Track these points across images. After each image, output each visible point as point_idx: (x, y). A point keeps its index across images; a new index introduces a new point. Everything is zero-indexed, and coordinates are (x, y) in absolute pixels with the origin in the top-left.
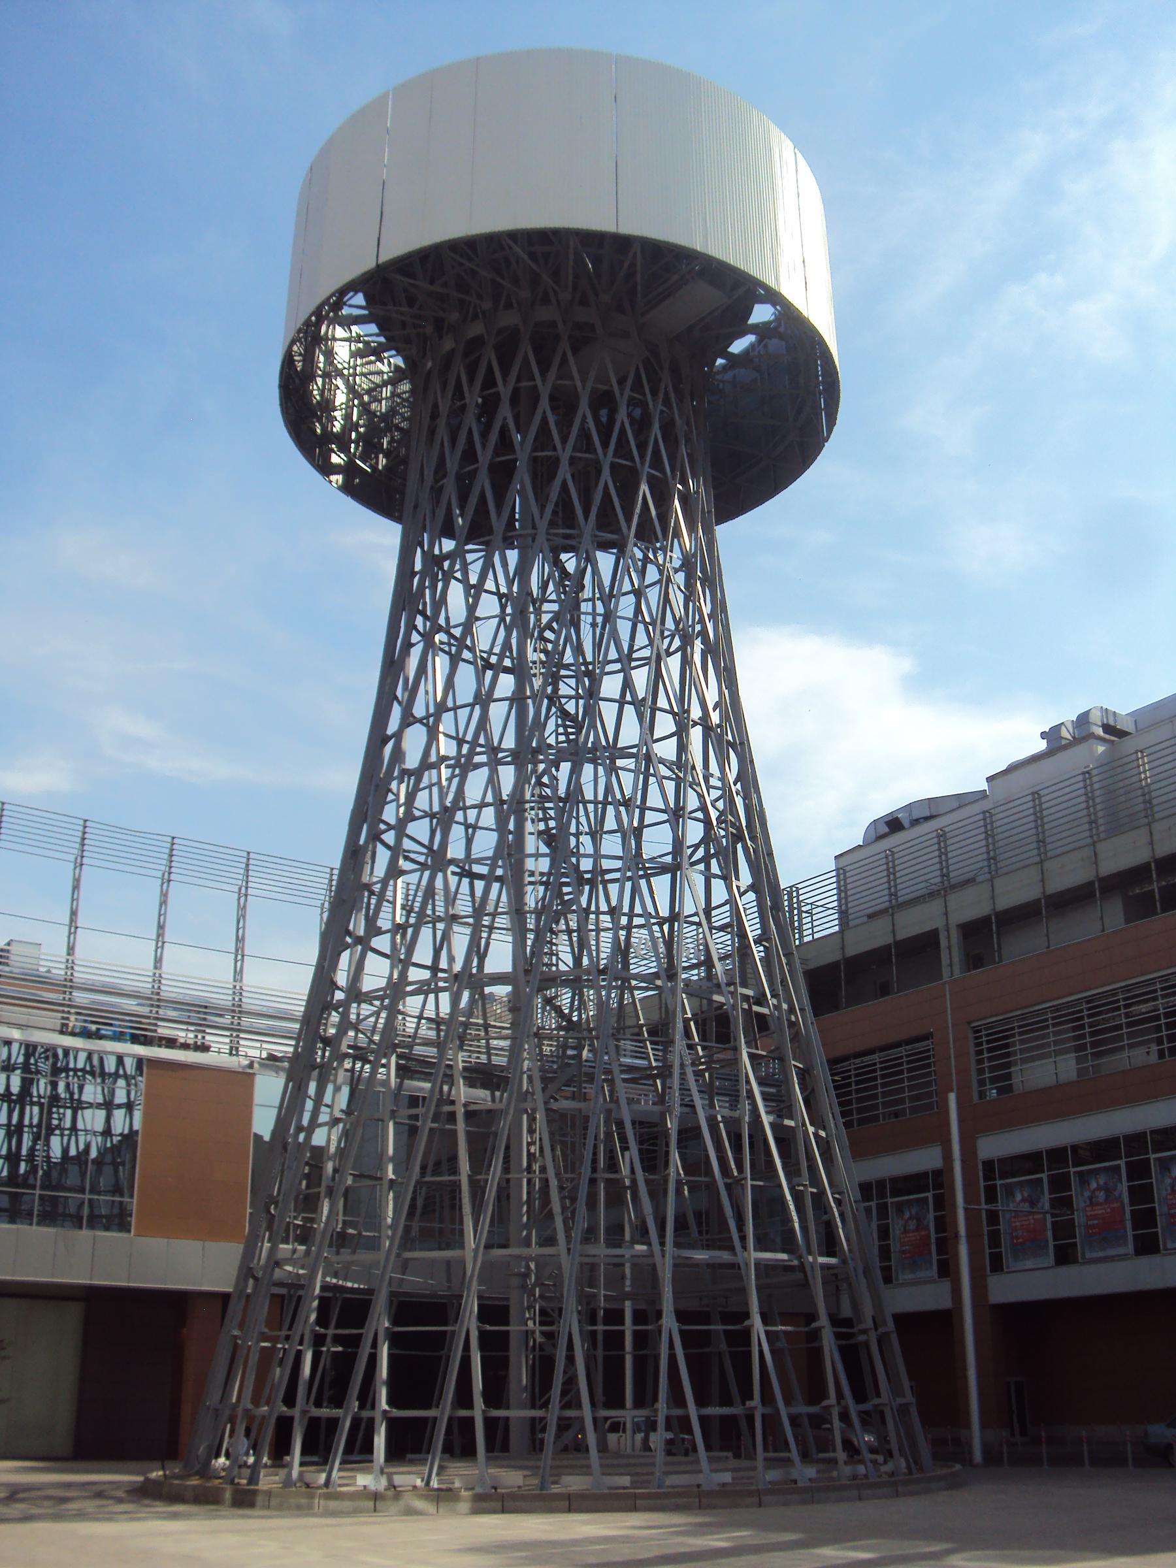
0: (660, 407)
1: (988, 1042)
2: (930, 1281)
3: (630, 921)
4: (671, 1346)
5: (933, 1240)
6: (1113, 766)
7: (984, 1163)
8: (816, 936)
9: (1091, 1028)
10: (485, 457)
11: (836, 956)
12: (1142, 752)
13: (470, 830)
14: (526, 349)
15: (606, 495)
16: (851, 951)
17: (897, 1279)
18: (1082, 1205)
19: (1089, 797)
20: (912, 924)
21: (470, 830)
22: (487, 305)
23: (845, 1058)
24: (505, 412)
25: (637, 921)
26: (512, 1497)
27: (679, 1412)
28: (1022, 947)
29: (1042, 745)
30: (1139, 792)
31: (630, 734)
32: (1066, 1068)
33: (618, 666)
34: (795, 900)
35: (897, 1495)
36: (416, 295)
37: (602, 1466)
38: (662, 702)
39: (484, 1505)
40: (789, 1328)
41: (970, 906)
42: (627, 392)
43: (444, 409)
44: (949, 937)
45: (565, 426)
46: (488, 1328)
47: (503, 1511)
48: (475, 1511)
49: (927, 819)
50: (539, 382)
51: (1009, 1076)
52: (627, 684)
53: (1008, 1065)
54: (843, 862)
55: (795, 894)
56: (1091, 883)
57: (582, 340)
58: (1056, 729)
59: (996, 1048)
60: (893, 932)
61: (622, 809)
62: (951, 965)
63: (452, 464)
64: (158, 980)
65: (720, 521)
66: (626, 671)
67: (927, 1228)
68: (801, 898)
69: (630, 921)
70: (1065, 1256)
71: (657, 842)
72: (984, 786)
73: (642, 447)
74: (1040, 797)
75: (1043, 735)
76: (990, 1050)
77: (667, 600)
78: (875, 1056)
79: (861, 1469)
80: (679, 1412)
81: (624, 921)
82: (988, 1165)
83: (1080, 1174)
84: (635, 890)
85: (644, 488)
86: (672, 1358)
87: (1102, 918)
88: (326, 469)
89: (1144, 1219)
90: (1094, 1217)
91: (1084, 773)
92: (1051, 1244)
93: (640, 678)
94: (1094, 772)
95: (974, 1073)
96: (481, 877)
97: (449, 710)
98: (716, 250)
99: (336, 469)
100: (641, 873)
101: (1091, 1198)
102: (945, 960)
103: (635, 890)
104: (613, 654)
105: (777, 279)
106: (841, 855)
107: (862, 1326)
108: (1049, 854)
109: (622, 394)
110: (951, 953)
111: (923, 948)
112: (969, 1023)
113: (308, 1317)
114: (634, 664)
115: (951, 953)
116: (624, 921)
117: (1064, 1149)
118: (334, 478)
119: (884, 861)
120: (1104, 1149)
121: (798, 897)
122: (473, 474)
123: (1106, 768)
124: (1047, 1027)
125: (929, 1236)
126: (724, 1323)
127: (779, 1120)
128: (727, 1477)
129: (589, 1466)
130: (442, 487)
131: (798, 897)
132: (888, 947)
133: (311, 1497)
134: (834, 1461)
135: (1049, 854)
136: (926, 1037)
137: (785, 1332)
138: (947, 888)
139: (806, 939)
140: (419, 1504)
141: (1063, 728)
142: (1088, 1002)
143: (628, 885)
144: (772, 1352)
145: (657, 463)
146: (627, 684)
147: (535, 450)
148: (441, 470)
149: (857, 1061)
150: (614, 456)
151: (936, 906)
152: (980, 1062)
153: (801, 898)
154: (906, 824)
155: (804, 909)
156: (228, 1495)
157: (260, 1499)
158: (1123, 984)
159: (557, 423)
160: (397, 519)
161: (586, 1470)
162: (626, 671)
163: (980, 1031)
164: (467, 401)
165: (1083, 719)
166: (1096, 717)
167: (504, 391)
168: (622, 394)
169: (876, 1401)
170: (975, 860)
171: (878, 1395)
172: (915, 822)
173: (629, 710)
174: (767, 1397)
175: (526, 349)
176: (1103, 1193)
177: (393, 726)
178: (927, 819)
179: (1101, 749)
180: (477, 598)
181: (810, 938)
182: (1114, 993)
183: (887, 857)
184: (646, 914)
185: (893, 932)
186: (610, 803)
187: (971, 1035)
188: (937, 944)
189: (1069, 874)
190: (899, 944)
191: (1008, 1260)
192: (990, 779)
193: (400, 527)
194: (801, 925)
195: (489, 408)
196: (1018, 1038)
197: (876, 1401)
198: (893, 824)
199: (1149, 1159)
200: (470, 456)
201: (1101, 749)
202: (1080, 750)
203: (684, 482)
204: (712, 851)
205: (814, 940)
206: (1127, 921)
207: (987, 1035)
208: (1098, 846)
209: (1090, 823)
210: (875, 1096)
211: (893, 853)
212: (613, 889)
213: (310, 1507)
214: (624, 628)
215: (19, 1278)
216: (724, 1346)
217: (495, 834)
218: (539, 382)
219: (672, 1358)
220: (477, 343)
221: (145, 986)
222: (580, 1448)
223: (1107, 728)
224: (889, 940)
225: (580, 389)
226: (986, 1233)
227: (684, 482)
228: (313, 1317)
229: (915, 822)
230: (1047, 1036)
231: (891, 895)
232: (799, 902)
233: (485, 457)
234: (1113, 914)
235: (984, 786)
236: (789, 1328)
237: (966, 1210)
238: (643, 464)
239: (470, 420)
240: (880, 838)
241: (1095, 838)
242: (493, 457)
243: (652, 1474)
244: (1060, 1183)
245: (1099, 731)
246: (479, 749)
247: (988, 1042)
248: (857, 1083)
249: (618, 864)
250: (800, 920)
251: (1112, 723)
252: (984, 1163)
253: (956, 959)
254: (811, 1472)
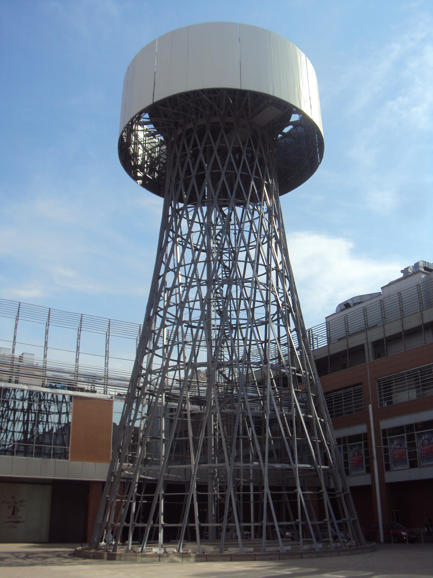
1: (383, 385)
5: (364, 459)
6: (426, 282)
8: (319, 347)
10: (194, 173)
16: (332, 352)
19: (419, 294)
20: (354, 342)
22: (194, 117)
23: (330, 392)
25: (253, 343)
26: (210, 556)
27: (271, 524)
29: (401, 275)
32: (412, 394)
33: (244, 249)
36: (168, 113)
38: (261, 262)
39: (199, 559)
40: (311, 492)
41: (376, 335)
44: (368, 347)
46: (200, 493)
47: (207, 561)
48: (197, 561)
49: (359, 303)
51: (391, 398)
52: (248, 255)
53: (391, 394)
54: (328, 319)
55: (311, 332)
56: (421, 326)
58: (406, 269)
59: (386, 388)
61: (247, 301)
63: (182, 175)
64: (77, 367)
66: (247, 251)
68: (313, 333)
70: (413, 465)
71: (260, 313)
72: (380, 291)
73: (252, 168)
75: (402, 271)
76: (384, 388)
77: (262, 224)
79: (339, 545)
81: (248, 342)
82: (384, 431)
88: (136, 178)
89: (412, 455)
91: (417, 285)
93: (253, 253)
94: (421, 285)
95: (378, 396)
96: (195, 327)
99: (139, 178)
100: (254, 325)
105: (300, 105)
108: (405, 315)
110: (369, 353)
112: (376, 378)
113: (134, 490)
114: (250, 248)
115: (369, 353)
116: (248, 342)
117: (412, 425)
118: (138, 181)
124: (405, 380)
126: (287, 491)
127: (306, 415)
128: (289, 548)
129: (238, 544)
133: (136, 556)
135: (405, 315)
137: (310, 494)
138: (367, 328)
139: (315, 348)
140: (176, 559)
143: (249, 329)
144: (305, 501)
145: (257, 174)
146: (248, 255)
148: (178, 178)
149: (335, 393)
150: (241, 171)
151: (363, 335)
153: (313, 333)
154: (351, 305)
156: (105, 556)
162: (247, 251)
163: (380, 381)
165: (417, 265)
166: (421, 264)
167: (201, 148)
168: (244, 149)
169: (344, 519)
171: (345, 517)
172: (355, 304)
173: (249, 265)
177: (162, 272)
178: (359, 303)
179: (423, 276)
180: (192, 224)
183: (344, 317)
184: (256, 340)
186: (242, 299)
187: (377, 383)
189: (412, 323)
191: (392, 466)
192: (382, 288)
194: (313, 343)
195: (195, 155)
198: (347, 305)
199: (362, 441)
200: (188, 172)
201: (423, 276)
203: (267, 181)
204: (280, 316)
205: (318, 349)
207: (383, 383)
212: (244, 331)
213: (136, 560)
214: (246, 235)
221: (72, 369)
223: (425, 268)
224: (346, 348)
225: (228, 147)
226: (383, 456)
228: (136, 490)
232: (312, 335)
233: (194, 173)
235: (380, 291)
236: (311, 492)
237: (376, 448)
238: (252, 174)
239: (188, 159)
240: (342, 310)
244: (411, 438)
246: (193, 280)
247: (383, 385)
249: (246, 322)
250: (313, 341)
251: (427, 266)
254: (320, 545)
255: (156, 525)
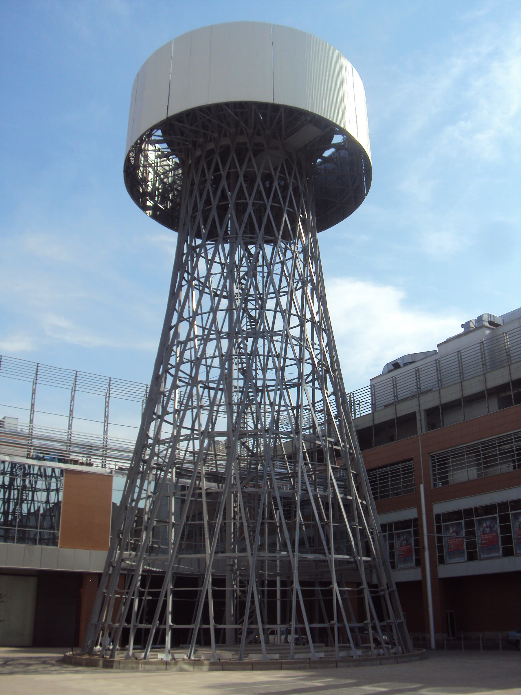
0: (293, 180)
1: (438, 462)
2: (412, 568)
3: (279, 408)
4: (297, 597)
5: (413, 550)
6: (493, 339)
7: (436, 515)
8: (362, 415)
9: (483, 456)
10: (215, 203)
11: (370, 424)
12: (506, 333)
13: (208, 368)
14: (233, 155)
15: (269, 219)
16: (377, 422)
17: (397, 567)
18: (480, 534)
19: (483, 353)
20: (404, 410)
21: (208, 368)
22: (216, 135)
23: (375, 469)
24: (224, 183)
25: (282, 408)
26: (227, 663)
27: (301, 626)
28: (453, 420)
29: (462, 330)
30: (505, 351)
31: (279, 325)
32: (472, 473)
33: (274, 295)
34: (352, 399)
35: (398, 663)
36: (184, 131)
37: (266, 650)
38: (293, 311)
39: (215, 667)
40: (350, 589)
41: (430, 401)
42: (278, 174)
43: (197, 181)
44: (420, 415)
45: (250, 189)
46: (216, 588)
47: (223, 670)
48: (211, 670)
49: (411, 363)
50: (239, 169)
51: (447, 477)
52: (278, 303)
53: (447, 472)
54: (374, 382)
55: (352, 396)
56: (483, 392)
57: (258, 151)
58: (468, 323)
59: (441, 464)
60: (396, 413)
61: (276, 358)
62: (421, 428)
63: (200, 206)
64: (70, 434)
65: (319, 231)
66: (277, 298)
67: (411, 544)
68: (355, 398)
69: (279, 408)
70: (472, 557)
72: (436, 348)
73: (284, 198)
74: (461, 353)
75: (462, 326)
76: (438, 465)
77: (295, 266)
78: (388, 468)
79: (382, 651)
80: (301, 626)
81: (276, 408)
82: (438, 516)
83: (478, 520)
84: (281, 395)
85: (285, 216)
86: (298, 602)
87: (488, 407)
88: (144, 208)
89: (507, 540)
90: (485, 539)
91: (480, 343)
92: (466, 551)
93: (284, 300)
94: (485, 342)
95: (431, 476)
96: (213, 389)
97: (199, 315)
98: (317, 111)
99: (149, 208)
100: (284, 387)
101: (483, 531)
102: (419, 425)
103: (281, 395)
104: (272, 290)
105: (344, 123)
106: (373, 379)
107: (382, 588)
108: (465, 379)
109: (275, 175)
110: (421, 422)
111: (409, 420)
112: (429, 453)
113: (136, 584)
114: (281, 294)
115: (421, 422)
116: (276, 408)
117: (472, 509)
118: (148, 212)
119: (392, 382)
120: (489, 509)
121: (353, 397)
122: (210, 210)
123: (490, 340)
124: (464, 455)
125: (411, 548)
126: (321, 587)
127: (345, 497)
128: (322, 655)
129: (261, 650)
130: (196, 216)
131: (353, 397)
132: (394, 420)
133: (138, 663)
134: (369, 648)
135: (465, 379)
136: (410, 460)
137: (348, 590)
138: (419, 394)
139: (357, 416)
140: (186, 667)
141: (471, 323)
142: (482, 444)
143: (278, 392)
144: (342, 599)
145: (291, 205)
146: (278, 303)
147: (237, 199)
148: (195, 208)
149: (380, 470)
150: (272, 202)
151: (415, 402)
152: (434, 471)
153: (355, 398)
154: (401, 365)
155: (356, 403)
156: (101, 663)
157: (115, 665)
158: (498, 436)
159: (247, 188)
160: (176, 230)
161: (260, 651)
162: (277, 298)
163: (434, 457)
164: (207, 178)
165: (480, 319)
166: (486, 318)
167: (223, 173)
168: (275, 175)
169: (388, 621)
170: (432, 381)
171: (389, 618)
172: (406, 364)
173: (279, 315)
174: (340, 619)
175: (233, 155)
176: (488, 529)
177: (174, 322)
178: (411, 363)
179: (488, 332)
180: (211, 265)
181: (359, 416)
182: (493, 440)
183: (393, 380)
184: (286, 405)
185: (396, 413)
186: (270, 356)
187: (430, 459)
188: (415, 418)
189: (473, 387)
190: (398, 419)
191: (446, 559)
192: (438, 345)
193: (177, 233)
194: (355, 410)
195: (217, 181)
196: (451, 460)
197: (388, 621)
198: (396, 365)
199: (509, 514)
200: (208, 202)
201: (488, 332)
202: (479, 332)
203: (303, 214)
204: (316, 377)
205: (361, 417)
206: (499, 408)
207: (437, 459)
208: (486, 375)
209: (483, 365)
210: (388, 486)
211: (396, 378)
212: (272, 394)
213: (137, 668)
214: (276, 279)
215: (8, 567)
216: (321, 597)
217: (219, 369)
218: (239, 169)
219: (298, 602)
220: (211, 152)
221: (64, 437)
222: (257, 642)
223: (491, 323)
224: (394, 417)
225: (257, 172)
226: (437, 546)
227: (303, 214)
228: (139, 584)
229: (406, 364)
230: (464, 459)
231: (395, 397)
232: (354, 400)
233: (215, 203)
234: (493, 405)
235: (436, 348)
236: (350, 589)
237: (428, 536)
238: (285, 206)
239: (208, 186)
240: (390, 371)
241: (485, 371)
242: (218, 203)
243: (289, 653)
244: (470, 525)
245: (487, 324)
246: (212, 332)
247: (438, 462)
248: (380, 480)
249: (274, 383)
250: (354, 408)
251: (492, 320)
252: (436, 515)
253: (424, 425)
254: (359, 652)
255: (162, 627)
